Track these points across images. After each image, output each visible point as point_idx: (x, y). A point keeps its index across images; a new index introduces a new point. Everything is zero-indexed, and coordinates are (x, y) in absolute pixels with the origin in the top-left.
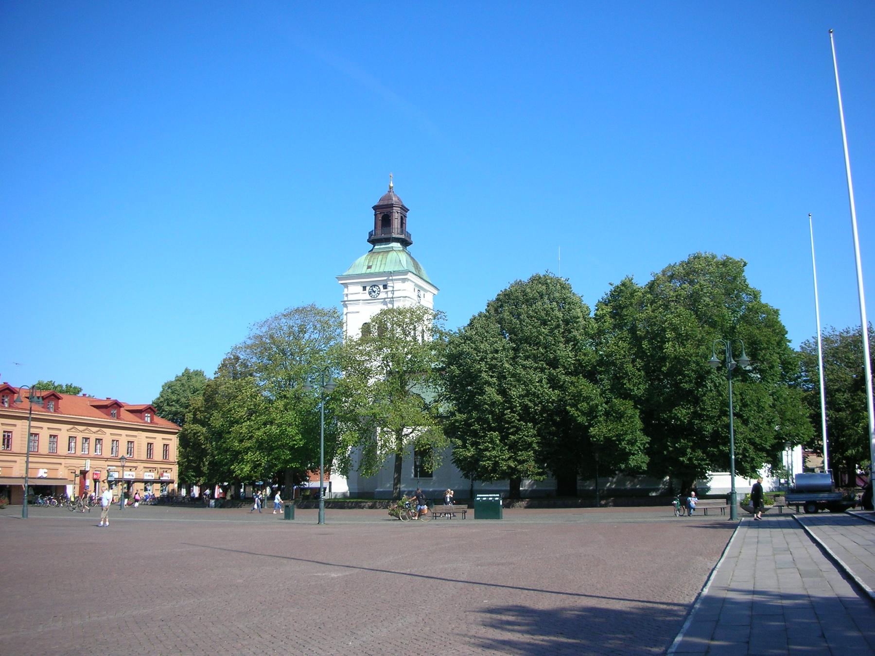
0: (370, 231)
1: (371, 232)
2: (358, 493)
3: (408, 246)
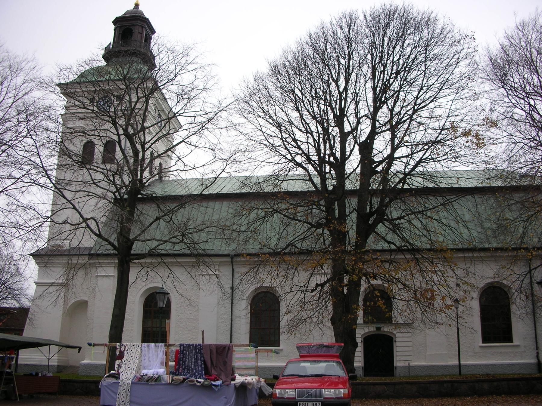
2: (58, 366)
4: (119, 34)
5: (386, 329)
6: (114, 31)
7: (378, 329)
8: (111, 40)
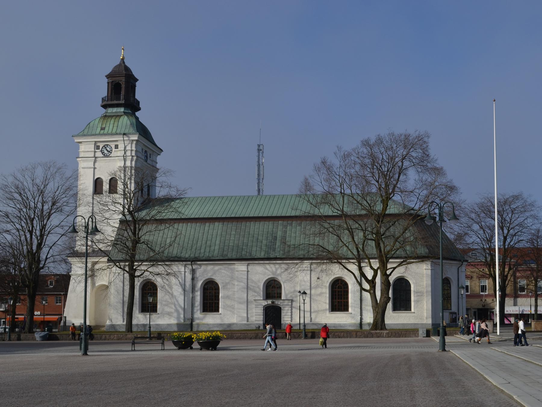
1: (104, 97)
4: (112, 87)
5: (278, 302)
7: (273, 302)
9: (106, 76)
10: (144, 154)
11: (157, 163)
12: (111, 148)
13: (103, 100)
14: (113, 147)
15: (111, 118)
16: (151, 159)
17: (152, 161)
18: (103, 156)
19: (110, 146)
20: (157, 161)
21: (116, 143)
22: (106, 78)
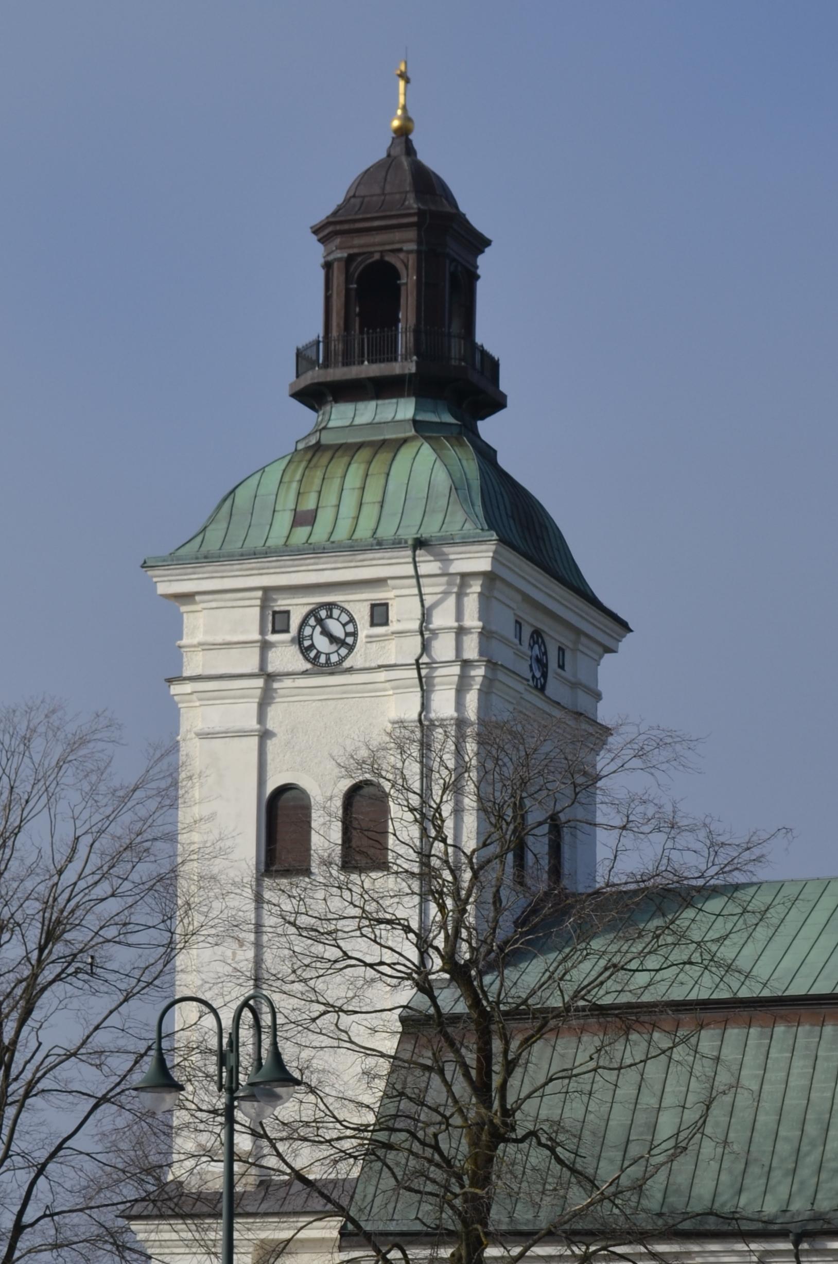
0: (301, 343)
1: (307, 347)
3: (483, 418)
4: (348, 291)
6: (321, 273)
8: (316, 330)
9: (316, 231)
10: (525, 648)
11: (598, 696)
12: (352, 620)
13: (303, 359)
14: (362, 614)
15: (345, 460)
16: (568, 673)
17: (575, 685)
18: (309, 666)
19: (343, 610)
20: (601, 687)
21: (378, 595)
22: (314, 238)
